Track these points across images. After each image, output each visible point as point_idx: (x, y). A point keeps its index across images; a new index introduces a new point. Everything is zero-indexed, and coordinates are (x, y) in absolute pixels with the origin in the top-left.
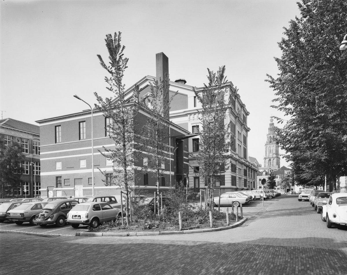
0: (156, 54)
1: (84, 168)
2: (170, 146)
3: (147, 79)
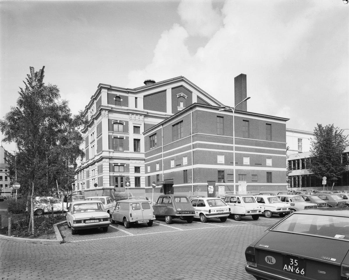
0: (246, 75)
1: (222, 164)
2: (162, 146)
3: (183, 80)
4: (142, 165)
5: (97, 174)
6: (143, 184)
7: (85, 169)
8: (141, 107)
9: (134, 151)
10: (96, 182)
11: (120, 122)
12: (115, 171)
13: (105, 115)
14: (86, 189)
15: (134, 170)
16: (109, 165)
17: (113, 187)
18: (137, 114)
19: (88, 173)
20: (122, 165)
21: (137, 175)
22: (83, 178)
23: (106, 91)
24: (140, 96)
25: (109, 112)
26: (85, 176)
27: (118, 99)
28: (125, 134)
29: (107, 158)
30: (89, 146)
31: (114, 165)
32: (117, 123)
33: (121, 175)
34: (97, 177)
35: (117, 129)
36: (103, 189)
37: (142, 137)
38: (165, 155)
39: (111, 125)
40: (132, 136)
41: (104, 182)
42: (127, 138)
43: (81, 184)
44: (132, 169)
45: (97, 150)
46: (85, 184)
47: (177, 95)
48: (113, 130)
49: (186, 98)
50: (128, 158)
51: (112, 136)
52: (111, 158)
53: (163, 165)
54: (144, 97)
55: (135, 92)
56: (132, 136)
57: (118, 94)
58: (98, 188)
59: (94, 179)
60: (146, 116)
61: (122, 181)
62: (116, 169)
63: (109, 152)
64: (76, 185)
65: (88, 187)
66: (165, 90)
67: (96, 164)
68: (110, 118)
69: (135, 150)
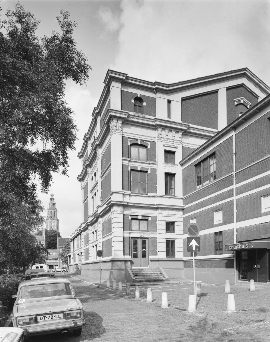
2: (234, 173)
3: (245, 74)
4: (178, 218)
5: (101, 237)
6: (179, 253)
7: (83, 233)
8: (176, 116)
9: (165, 194)
10: (100, 248)
11: (143, 143)
12: (132, 229)
13: (117, 129)
14: (84, 261)
15: (164, 227)
16: (124, 218)
17: (128, 257)
18: (171, 129)
19: (87, 237)
20: (145, 219)
21: (170, 236)
22: (81, 245)
23: (119, 85)
24: (177, 98)
25: (123, 123)
26: (82, 243)
27: (138, 104)
28: (150, 164)
29: (119, 205)
30: (88, 198)
31: (132, 219)
32: (137, 144)
33: (142, 237)
34: (100, 241)
35: (137, 154)
36: (113, 261)
37: (178, 170)
38: (239, 191)
39: (129, 146)
40: (162, 167)
41: (113, 249)
42: (154, 171)
43: (78, 254)
44: (161, 226)
45: (102, 198)
46: (83, 254)
47: (234, 101)
48: (129, 156)
49: (248, 106)
50: (156, 205)
51: (128, 166)
52: (126, 206)
53: (235, 211)
54: (182, 100)
55: (167, 89)
56: (162, 167)
57: (139, 93)
58: (102, 259)
59: (96, 246)
60: (186, 133)
61: (144, 247)
62: (135, 225)
63: (124, 194)
64: (72, 256)
65: (87, 258)
66: (216, 92)
67: (100, 220)
68: (126, 135)
69: (166, 192)
